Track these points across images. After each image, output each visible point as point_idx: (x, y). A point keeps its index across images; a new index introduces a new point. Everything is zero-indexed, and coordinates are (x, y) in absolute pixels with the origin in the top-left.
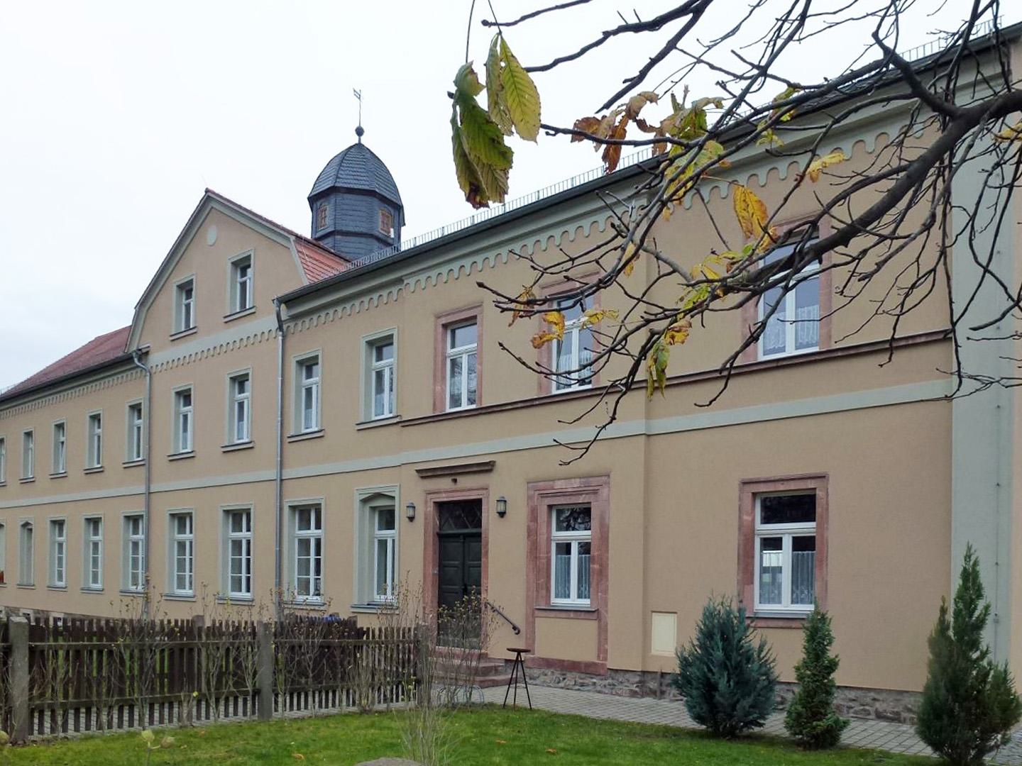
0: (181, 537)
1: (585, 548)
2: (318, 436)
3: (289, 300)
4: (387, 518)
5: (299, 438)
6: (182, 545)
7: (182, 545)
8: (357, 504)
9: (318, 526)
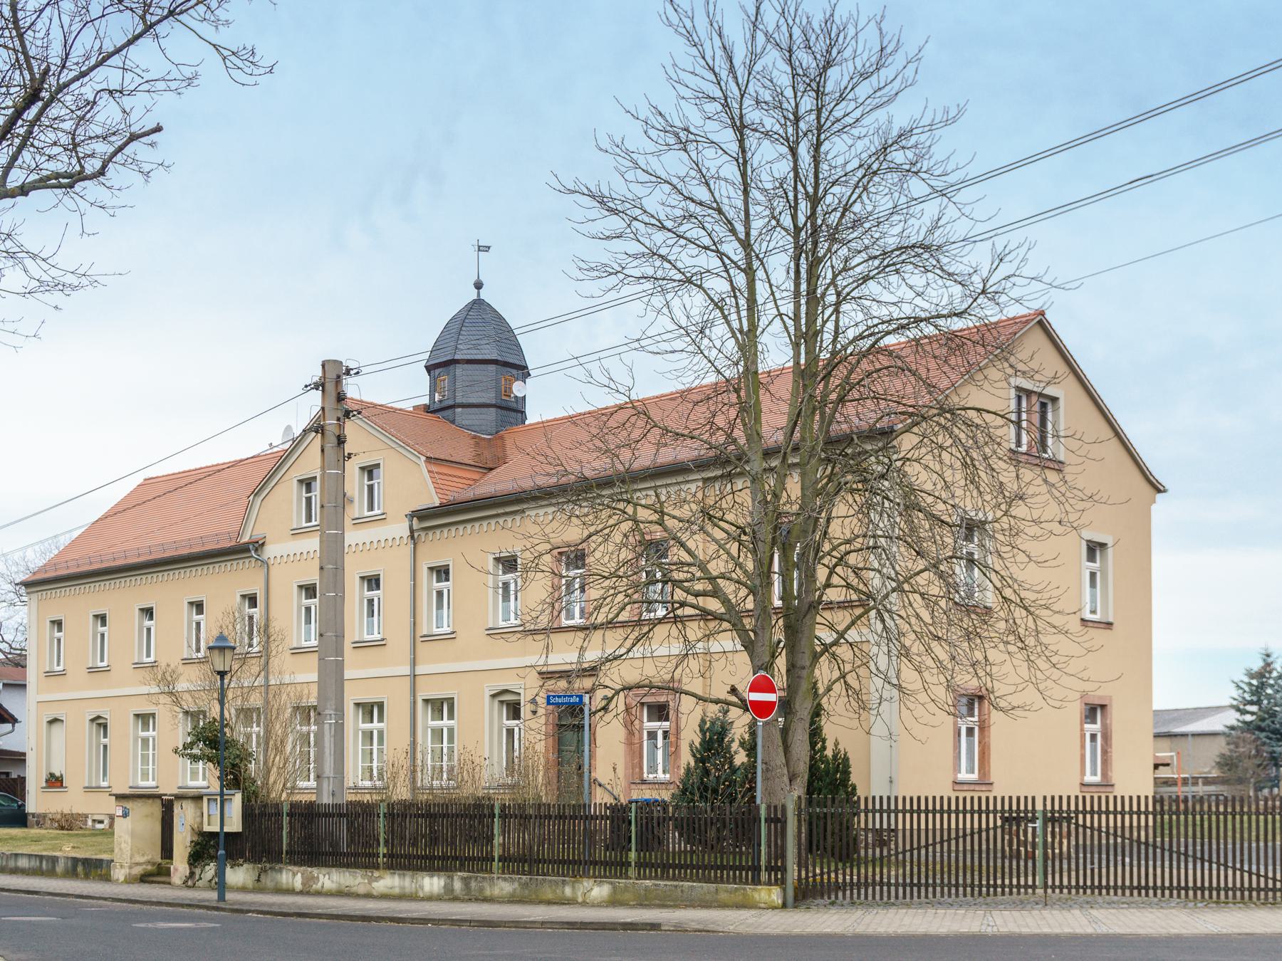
0: (145, 734)
1: (666, 734)
2: (451, 637)
3: (421, 515)
4: (514, 710)
5: (429, 638)
6: (145, 741)
7: (145, 741)
8: (487, 699)
9: (451, 716)
